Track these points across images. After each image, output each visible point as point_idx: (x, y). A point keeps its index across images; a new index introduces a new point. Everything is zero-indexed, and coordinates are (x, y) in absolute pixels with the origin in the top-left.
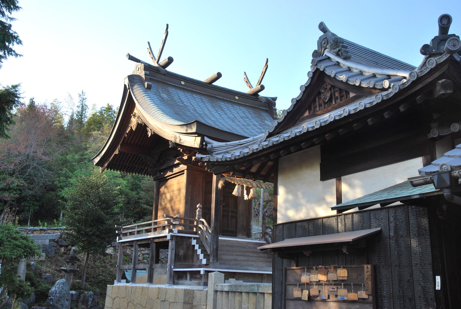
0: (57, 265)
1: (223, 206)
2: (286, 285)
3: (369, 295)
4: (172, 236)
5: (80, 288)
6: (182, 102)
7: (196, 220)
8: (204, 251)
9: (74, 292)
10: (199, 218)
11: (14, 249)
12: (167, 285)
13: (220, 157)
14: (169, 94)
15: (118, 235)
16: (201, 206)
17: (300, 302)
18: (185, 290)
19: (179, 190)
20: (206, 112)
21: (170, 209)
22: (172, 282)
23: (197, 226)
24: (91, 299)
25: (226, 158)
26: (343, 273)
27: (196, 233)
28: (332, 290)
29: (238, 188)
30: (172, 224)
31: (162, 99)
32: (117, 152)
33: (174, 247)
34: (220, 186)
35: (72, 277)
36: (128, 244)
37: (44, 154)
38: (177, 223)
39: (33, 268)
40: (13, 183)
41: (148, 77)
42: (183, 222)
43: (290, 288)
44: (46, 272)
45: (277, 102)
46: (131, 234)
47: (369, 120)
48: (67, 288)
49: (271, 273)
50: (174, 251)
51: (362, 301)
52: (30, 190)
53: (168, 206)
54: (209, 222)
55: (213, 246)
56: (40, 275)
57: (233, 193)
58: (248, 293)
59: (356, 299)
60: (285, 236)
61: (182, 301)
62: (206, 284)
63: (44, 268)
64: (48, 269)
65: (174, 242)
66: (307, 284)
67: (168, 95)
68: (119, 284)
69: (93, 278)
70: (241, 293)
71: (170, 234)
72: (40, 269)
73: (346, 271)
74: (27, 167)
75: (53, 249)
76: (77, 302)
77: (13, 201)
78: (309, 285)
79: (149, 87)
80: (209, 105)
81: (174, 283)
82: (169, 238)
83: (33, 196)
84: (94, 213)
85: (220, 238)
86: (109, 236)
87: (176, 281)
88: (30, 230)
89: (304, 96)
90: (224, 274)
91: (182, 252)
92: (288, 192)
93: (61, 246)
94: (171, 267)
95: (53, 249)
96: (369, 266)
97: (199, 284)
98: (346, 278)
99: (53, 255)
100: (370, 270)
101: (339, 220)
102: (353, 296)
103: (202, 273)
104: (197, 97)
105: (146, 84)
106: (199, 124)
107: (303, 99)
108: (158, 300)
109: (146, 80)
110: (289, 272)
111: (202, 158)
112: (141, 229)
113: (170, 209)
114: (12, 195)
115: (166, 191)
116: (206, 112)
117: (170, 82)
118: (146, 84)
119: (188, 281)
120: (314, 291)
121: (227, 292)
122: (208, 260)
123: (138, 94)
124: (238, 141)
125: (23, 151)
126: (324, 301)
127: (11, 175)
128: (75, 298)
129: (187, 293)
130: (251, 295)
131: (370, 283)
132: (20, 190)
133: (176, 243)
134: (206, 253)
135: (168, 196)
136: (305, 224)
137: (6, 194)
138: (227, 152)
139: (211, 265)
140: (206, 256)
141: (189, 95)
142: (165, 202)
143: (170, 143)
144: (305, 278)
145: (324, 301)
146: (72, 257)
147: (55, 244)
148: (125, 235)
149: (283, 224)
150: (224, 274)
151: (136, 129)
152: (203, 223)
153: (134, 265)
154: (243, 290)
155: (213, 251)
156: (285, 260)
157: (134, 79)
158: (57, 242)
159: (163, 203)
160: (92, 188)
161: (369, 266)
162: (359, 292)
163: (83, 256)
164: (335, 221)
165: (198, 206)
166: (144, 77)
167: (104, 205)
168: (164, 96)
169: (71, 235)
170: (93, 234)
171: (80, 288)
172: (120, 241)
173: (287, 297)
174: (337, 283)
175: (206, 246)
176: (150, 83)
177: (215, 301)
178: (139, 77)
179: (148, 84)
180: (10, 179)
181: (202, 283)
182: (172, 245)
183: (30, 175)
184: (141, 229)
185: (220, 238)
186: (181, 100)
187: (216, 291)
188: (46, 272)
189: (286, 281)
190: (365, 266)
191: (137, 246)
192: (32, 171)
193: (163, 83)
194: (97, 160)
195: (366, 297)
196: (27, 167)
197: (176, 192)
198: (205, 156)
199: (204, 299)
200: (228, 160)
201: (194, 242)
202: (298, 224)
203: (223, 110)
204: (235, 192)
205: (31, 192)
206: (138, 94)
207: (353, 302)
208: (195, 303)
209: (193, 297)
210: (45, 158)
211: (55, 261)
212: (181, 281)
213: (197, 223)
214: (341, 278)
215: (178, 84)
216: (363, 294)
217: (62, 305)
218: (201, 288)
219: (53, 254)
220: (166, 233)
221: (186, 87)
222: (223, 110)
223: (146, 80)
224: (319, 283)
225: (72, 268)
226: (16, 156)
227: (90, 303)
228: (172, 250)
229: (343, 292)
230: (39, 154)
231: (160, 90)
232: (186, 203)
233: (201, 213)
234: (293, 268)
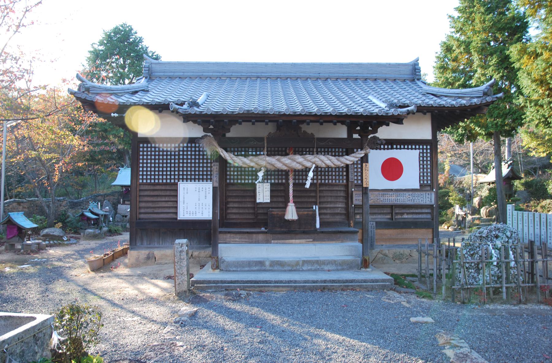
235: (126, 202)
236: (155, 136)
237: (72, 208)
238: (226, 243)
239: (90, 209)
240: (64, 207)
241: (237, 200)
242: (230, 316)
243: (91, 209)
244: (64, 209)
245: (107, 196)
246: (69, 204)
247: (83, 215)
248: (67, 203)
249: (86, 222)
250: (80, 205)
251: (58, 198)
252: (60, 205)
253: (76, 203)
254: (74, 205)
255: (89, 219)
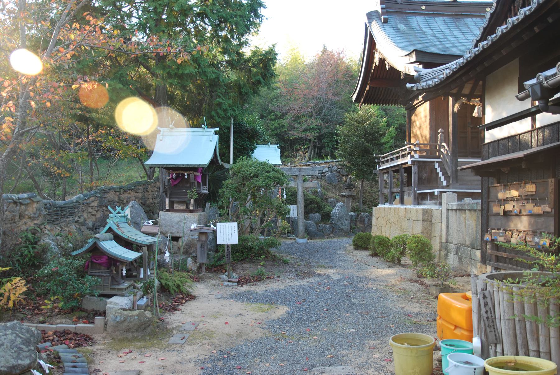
0: (340, 192)
1: (472, 128)
2: (489, 202)
3: (552, 209)
4: (413, 162)
5: (358, 210)
6: (421, 29)
7: (438, 145)
8: (445, 174)
9: (353, 213)
10: (441, 143)
11: (266, 179)
12: (412, 205)
13: (424, 84)
14: (407, 23)
15: (378, 163)
16: (443, 131)
17: (499, 217)
18: (423, 210)
19: (426, 117)
20: (447, 34)
21: (420, 136)
22: (417, 203)
23: (439, 150)
24: (367, 219)
25: (429, 85)
26: (531, 188)
27: (439, 157)
28: (522, 205)
29: (478, 109)
30: (413, 150)
31: (398, 31)
32: (368, 88)
33: (417, 171)
34: (456, 109)
35: (351, 201)
36: (385, 171)
37: (334, 95)
38: (418, 149)
39: (320, 194)
40: (312, 123)
41: (385, 10)
42: (428, 148)
43: (492, 204)
44: (330, 198)
45: (329, 49)
46: (387, 161)
47: (535, 28)
48: (344, 210)
49: (480, 191)
50: (417, 175)
51: (545, 214)
52: (327, 128)
53: (418, 133)
54: (448, 147)
55: (452, 168)
56: (327, 199)
57: (473, 115)
58: (470, 210)
59: (542, 212)
60: (490, 155)
61: (421, 219)
62: (440, 204)
63: (329, 194)
64: (333, 195)
65: (416, 167)
66: (504, 200)
67: (405, 25)
68: (382, 206)
69: (371, 201)
70: (465, 210)
71: (412, 159)
72: (326, 195)
73: (534, 186)
74: (322, 108)
75: (336, 178)
76: (356, 221)
77: (315, 139)
78: (505, 201)
79: (386, 21)
80: (452, 26)
81: (419, 204)
82: (410, 163)
83: (330, 133)
84: (361, 145)
85: (459, 160)
86: (372, 164)
87: (420, 202)
88: (316, 163)
89: (499, 7)
90: (456, 194)
91: (425, 176)
92: (494, 109)
93: (343, 175)
94: (414, 189)
95: (336, 178)
96: (553, 180)
97: (436, 204)
98: (534, 193)
99: (337, 183)
100: (553, 184)
101: (533, 135)
102: (537, 210)
103: (436, 194)
104: (439, 20)
105: (382, 18)
106: (418, 52)
107: (498, 11)
108: (405, 219)
109: (383, 14)
110: (491, 189)
111: (412, 87)
112: (393, 157)
113: (420, 136)
114: (313, 134)
115: (416, 118)
116: (447, 34)
117: (409, 10)
118: (382, 18)
119: (428, 202)
120: (508, 207)
121: (456, 210)
122: (448, 182)
123: (376, 29)
124: (444, 66)
125: (316, 94)
126: (517, 215)
127: (311, 117)
128: (354, 218)
129: (425, 212)
130: (473, 212)
131: (553, 197)
132: (319, 129)
133: (419, 167)
134: (446, 175)
135: (418, 123)
136: (506, 141)
137: (309, 134)
138: (434, 78)
139: (451, 186)
140: (447, 178)
141: (430, 19)
142: (415, 130)
143: (402, 74)
144: (501, 195)
145: (517, 215)
146: (348, 184)
147: (338, 174)
148: (383, 162)
149: (489, 143)
150: (456, 194)
151: (379, 64)
152: (443, 146)
153: (391, 189)
154: (467, 208)
155: (453, 173)
156: (490, 178)
157: (372, 15)
158: (339, 172)
159: (414, 131)
160: (359, 123)
161: (553, 180)
162: (543, 206)
163: (358, 183)
164: (529, 137)
165: (439, 131)
166: (380, 11)
167: (370, 137)
168: (402, 26)
169: (345, 165)
170: (363, 164)
171: (358, 210)
172: (380, 168)
173: (490, 213)
174: (527, 198)
175: (447, 168)
176: (386, 17)
177: (447, 218)
178: (377, 12)
179: (384, 19)
180: (310, 121)
181: (438, 203)
182: (415, 170)
183: (325, 115)
184: (393, 157)
185: (459, 160)
186: (420, 27)
187: (448, 210)
188: (330, 198)
189: (489, 198)
190: (550, 180)
191: (392, 173)
192: (326, 112)
193: (402, 13)
194: (354, 97)
195: (549, 210)
196: (322, 108)
197: (423, 119)
198: (413, 85)
199: (439, 217)
200: (431, 86)
201: (436, 166)
202: (500, 142)
203: (469, 28)
204: (475, 114)
205: (327, 130)
206: (376, 29)
207: (539, 215)
208: (433, 221)
209: (432, 216)
210: (336, 98)
211: (339, 188)
212: (424, 202)
213: (440, 148)
214: (529, 193)
215: (418, 10)
216: (547, 208)
217: (342, 224)
218: (437, 207)
219: (336, 182)
220: (408, 160)
221: (428, 11)
222: (469, 28)
223: (383, 14)
224: (513, 199)
225: (349, 194)
226: (312, 100)
227: (366, 222)
228: (415, 174)
229: (530, 206)
230: (330, 96)
231: (397, 21)
232: (431, 128)
233: (443, 137)
234: (495, 185)
235: (177, 207)
236: (141, 135)
237: (52, 222)
238: (482, 230)
239: (110, 230)
240: (32, 219)
241: (518, 332)
242: (149, 154)
243: (115, 228)
244: (31, 224)
245: (125, 191)
246: (44, 212)
247: (96, 249)
248: (39, 209)
249: (103, 271)
250: (72, 214)
251: (15, 196)
252: (21, 216)
253: (62, 208)
254: (57, 214)
255: (113, 262)
